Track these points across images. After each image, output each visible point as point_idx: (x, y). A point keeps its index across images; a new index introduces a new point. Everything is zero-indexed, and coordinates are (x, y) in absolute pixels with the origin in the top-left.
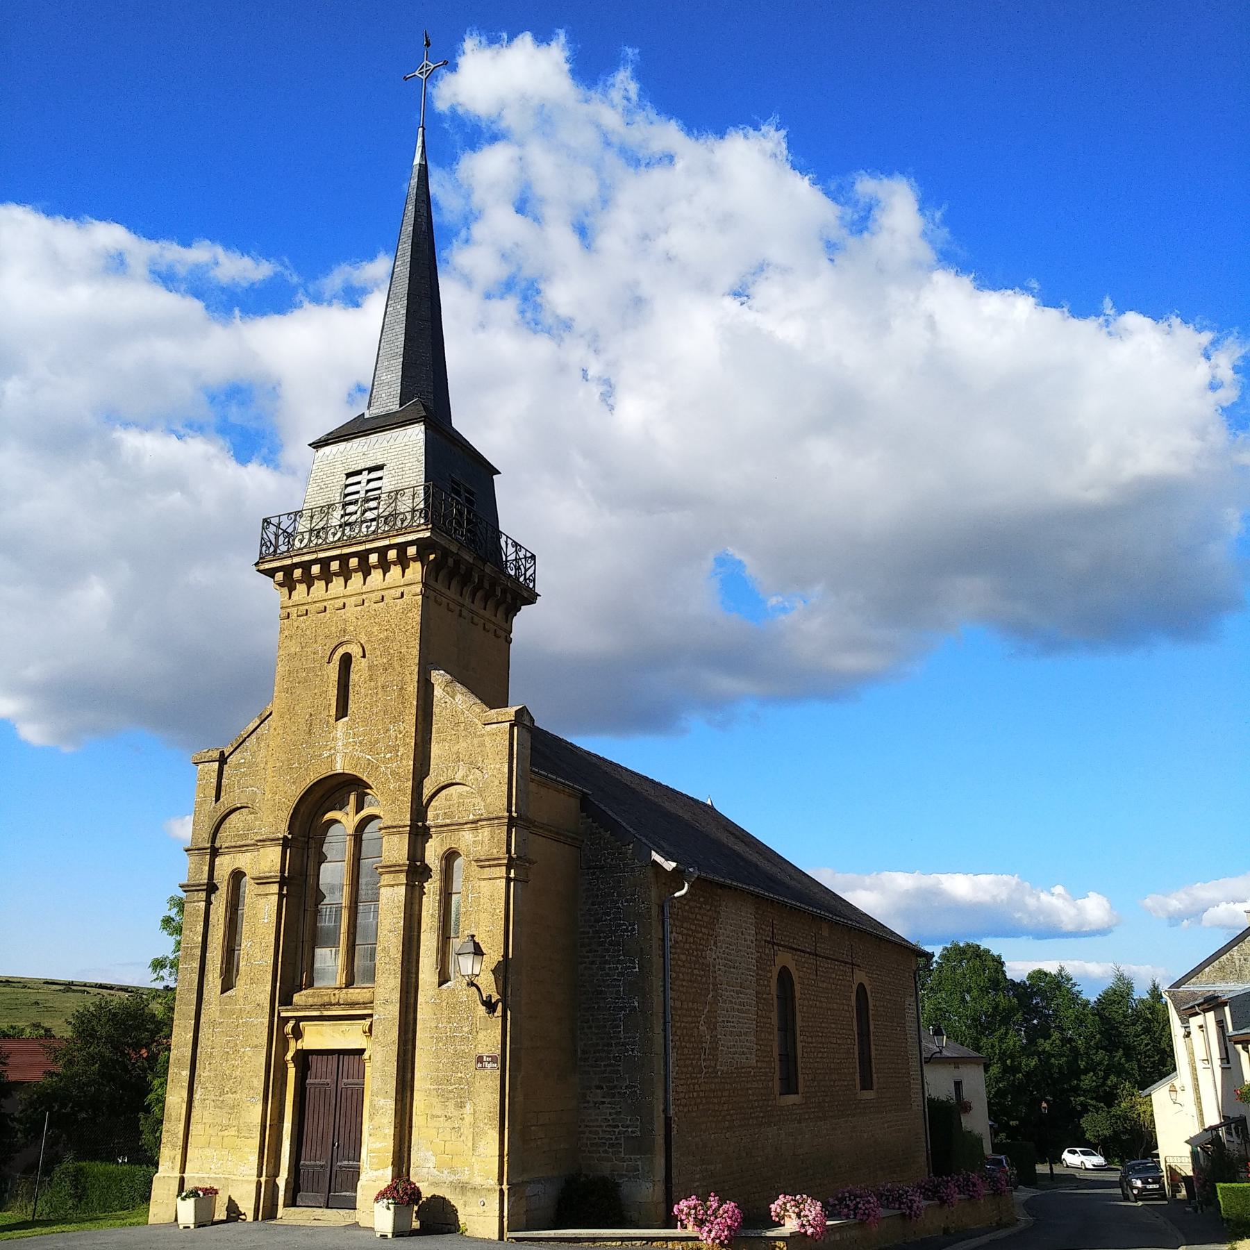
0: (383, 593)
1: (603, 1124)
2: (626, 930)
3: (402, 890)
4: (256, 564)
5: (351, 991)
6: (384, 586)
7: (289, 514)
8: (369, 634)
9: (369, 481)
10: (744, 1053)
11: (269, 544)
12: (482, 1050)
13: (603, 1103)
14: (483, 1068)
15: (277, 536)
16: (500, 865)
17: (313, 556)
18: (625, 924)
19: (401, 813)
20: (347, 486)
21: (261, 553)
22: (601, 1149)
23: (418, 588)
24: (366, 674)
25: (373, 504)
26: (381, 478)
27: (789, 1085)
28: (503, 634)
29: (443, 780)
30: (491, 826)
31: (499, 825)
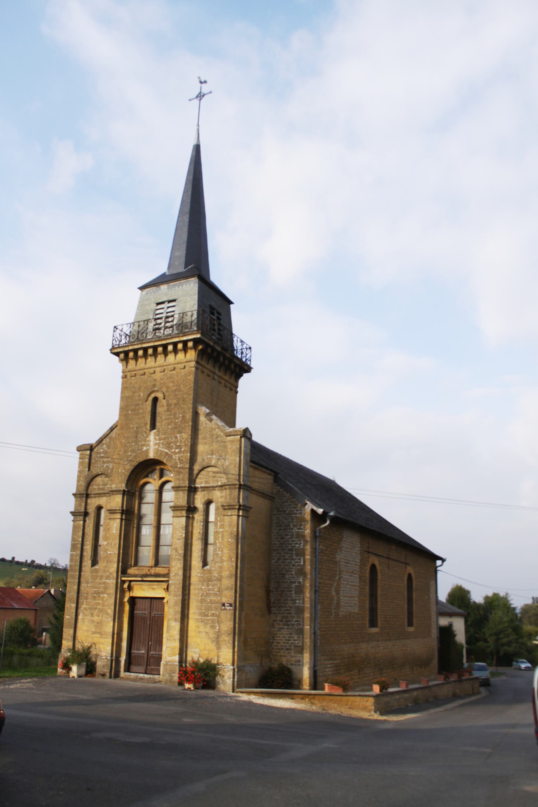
0: (175, 366)
1: (283, 639)
2: (297, 544)
3: (184, 520)
4: (111, 350)
5: (157, 569)
6: (176, 361)
7: (127, 324)
8: (168, 387)
9: (168, 307)
10: (352, 606)
11: (116, 339)
12: (224, 600)
13: (283, 628)
14: (225, 609)
15: (121, 336)
16: (235, 509)
17: (140, 346)
18: (296, 541)
19: (183, 480)
20: (157, 310)
21: (113, 344)
22: (282, 651)
23: (193, 364)
24: (165, 408)
25: (170, 319)
26: (174, 306)
27: (373, 623)
28: (234, 389)
29: (205, 464)
30: (230, 489)
31: (234, 488)
